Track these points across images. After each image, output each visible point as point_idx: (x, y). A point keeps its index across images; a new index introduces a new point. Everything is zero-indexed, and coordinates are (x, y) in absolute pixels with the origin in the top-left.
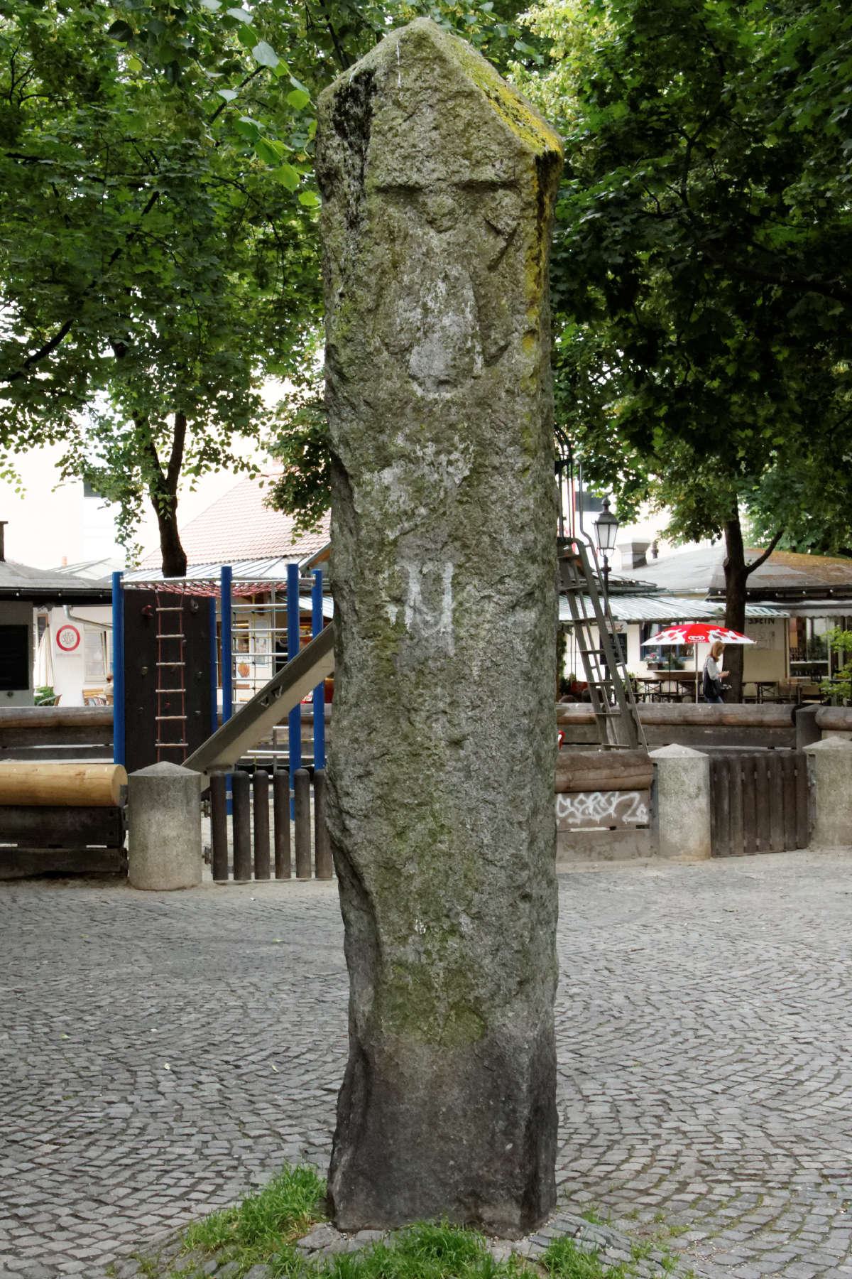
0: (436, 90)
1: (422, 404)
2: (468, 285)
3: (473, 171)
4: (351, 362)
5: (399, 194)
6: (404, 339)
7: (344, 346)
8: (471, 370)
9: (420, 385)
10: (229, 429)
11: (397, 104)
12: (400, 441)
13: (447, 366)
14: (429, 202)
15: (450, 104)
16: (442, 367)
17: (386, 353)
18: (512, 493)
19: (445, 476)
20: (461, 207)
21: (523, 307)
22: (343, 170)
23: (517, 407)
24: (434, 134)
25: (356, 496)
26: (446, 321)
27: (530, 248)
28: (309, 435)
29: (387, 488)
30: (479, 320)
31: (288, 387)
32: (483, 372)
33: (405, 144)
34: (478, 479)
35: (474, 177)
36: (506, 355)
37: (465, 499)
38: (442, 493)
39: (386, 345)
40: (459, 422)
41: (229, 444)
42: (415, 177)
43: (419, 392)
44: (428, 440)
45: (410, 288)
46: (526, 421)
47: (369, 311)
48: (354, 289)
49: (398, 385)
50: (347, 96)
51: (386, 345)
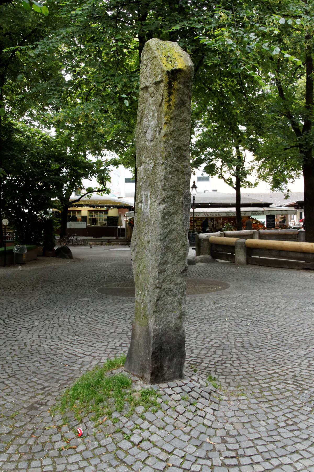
8: (156, 136)
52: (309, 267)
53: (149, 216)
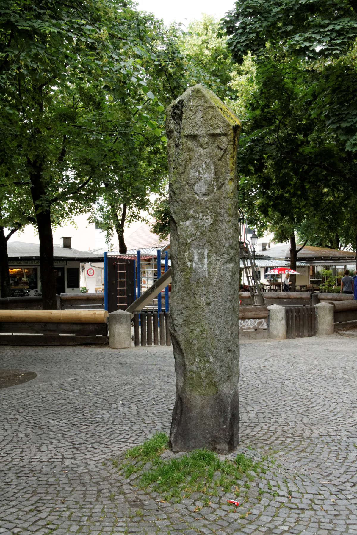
0: (202, 106)
4: (177, 189)
5: (191, 138)
8: (213, 191)
10: (140, 209)
11: (191, 110)
12: (191, 212)
14: (200, 140)
15: (207, 110)
17: (187, 186)
18: (226, 228)
24: (202, 119)
26: (206, 176)
29: (188, 227)
31: (158, 196)
43: (197, 197)
47: (182, 173)
52: (89, 341)
53: (207, 276)
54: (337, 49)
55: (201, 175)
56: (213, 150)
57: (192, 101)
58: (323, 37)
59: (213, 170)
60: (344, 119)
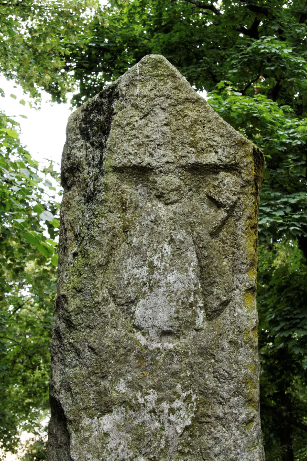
0: (168, 97)
1: (145, 352)
2: (191, 248)
3: (198, 156)
4: (79, 310)
5: (132, 174)
6: (131, 292)
7: (74, 296)
8: (194, 323)
9: (144, 334)
10: (6, 451)
11: (136, 107)
12: (121, 387)
13: (170, 318)
14: (159, 180)
15: (179, 108)
16: (166, 318)
17: (112, 304)
18: (236, 446)
19: (167, 424)
20: (186, 185)
21: (244, 267)
22: (84, 162)
23: (240, 358)
24: (165, 129)
25: (73, 442)
26: (171, 278)
27: (249, 218)
28: (37, 453)
29: (106, 435)
30: (201, 278)
31: (31, 435)
32: (205, 326)
33: (140, 136)
34: (200, 428)
35: (200, 161)
36: (227, 309)
37: (186, 450)
38: (163, 442)
39: (114, 296)
40: (181, 370)
41: (5, 457)
42: (147, 160)
43: (143, 341)
44: (150, 387)
45: (138, 248)
46: (249, 371)
47: (100, 266)
48: (87, 247)
49: (123, 333)
50: (92, 110)
51: (114, 296)
54: (295, 225)
55: (156, 276)
56: (194, 208)
57: (139, 86)
58: (275, 211)
59: (195, 263)
60: (299, 326)
